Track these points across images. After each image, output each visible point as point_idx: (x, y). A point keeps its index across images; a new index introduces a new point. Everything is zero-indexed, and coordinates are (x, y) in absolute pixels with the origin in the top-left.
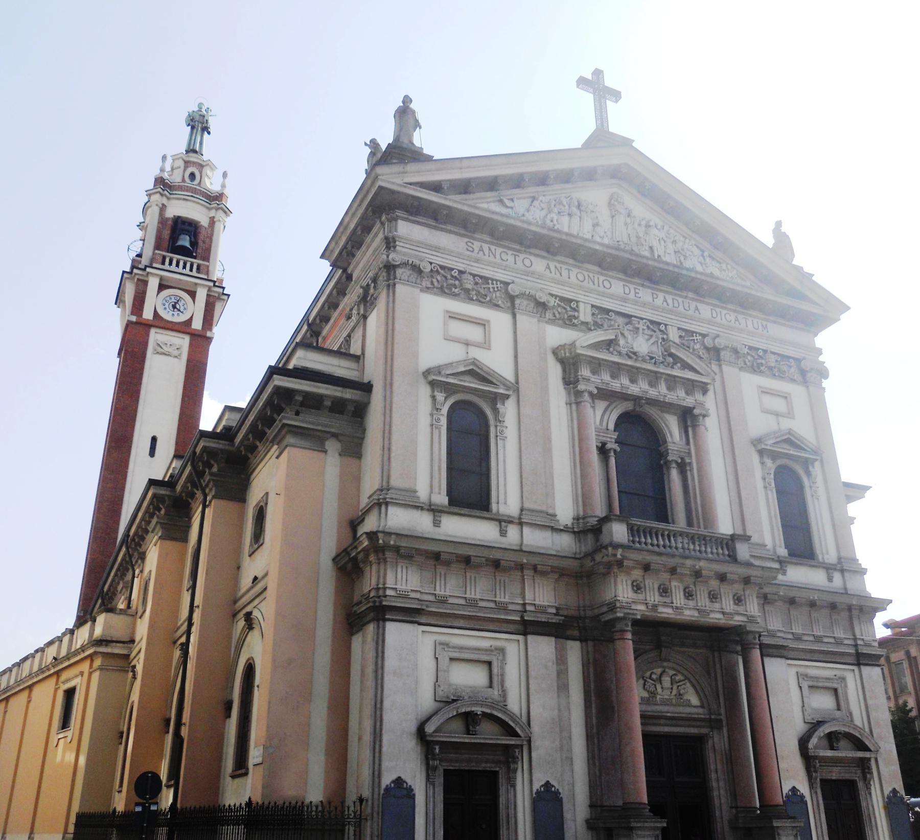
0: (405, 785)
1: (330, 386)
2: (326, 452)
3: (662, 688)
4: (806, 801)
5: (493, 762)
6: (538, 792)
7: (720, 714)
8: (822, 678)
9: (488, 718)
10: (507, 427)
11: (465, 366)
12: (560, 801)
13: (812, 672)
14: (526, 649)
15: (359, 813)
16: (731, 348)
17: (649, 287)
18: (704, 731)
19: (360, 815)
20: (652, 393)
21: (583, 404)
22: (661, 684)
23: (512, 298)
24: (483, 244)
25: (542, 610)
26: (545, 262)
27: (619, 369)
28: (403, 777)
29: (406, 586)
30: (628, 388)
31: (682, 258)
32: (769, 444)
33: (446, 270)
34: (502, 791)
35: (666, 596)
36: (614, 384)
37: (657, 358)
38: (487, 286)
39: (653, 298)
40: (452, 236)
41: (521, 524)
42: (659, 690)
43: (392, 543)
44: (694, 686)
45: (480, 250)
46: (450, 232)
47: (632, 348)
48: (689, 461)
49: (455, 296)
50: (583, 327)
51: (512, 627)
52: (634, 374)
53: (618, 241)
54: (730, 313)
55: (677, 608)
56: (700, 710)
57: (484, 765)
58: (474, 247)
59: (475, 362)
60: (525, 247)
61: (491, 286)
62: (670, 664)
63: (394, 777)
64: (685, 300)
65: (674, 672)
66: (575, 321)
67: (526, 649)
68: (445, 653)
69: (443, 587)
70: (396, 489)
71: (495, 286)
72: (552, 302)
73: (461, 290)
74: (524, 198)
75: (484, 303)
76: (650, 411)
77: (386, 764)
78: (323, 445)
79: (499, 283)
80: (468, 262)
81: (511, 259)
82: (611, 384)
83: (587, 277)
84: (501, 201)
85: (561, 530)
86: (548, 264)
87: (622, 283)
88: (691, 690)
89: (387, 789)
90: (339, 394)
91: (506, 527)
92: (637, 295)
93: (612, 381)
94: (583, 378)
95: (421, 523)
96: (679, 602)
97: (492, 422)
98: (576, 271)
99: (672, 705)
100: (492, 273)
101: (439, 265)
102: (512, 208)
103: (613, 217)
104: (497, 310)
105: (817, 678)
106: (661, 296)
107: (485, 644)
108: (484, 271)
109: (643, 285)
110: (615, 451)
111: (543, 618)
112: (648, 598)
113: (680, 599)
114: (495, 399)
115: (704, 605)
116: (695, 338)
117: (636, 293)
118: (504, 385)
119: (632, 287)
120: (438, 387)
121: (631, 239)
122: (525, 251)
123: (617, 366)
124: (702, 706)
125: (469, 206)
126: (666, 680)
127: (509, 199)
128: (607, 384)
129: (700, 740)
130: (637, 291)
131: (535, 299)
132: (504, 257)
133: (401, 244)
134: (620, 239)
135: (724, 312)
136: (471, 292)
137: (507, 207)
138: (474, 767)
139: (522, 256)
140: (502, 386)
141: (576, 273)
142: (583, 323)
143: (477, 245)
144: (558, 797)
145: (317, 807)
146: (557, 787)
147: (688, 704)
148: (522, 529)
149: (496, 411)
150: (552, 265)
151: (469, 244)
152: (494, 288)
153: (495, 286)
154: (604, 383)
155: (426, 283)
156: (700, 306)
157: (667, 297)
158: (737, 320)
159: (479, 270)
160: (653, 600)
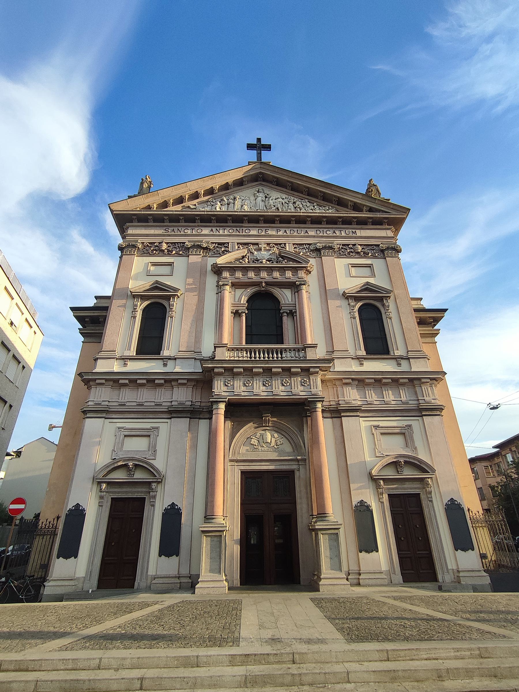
9: (409, 464)
13: (382, 424)
15: (55, 525)
18: (294, 467)
23: (382, 251)
24: (212, 228)
33: (346, 246)
37: (273, 260)
38: (175, 246)
41: (408, 359)
59: (157, 282)
61: (177, 246)
73: (355, 253)
79: (307, 245)
86: (212, 229)
92: (267, 233)
95: (355, 367)
97: (383, 311)
101: (148, 242)
107: (148, 426)
114: (381, 299)
116: (305, 247)
117: (266, 232)
120: (98, 299)
123: (258, 269)
129: (291, 473)
135: (325, 230)
136: (360, 253)
144: (460, 507)
145: (25, 520)
148: (409, 361)
149: (383, 305)
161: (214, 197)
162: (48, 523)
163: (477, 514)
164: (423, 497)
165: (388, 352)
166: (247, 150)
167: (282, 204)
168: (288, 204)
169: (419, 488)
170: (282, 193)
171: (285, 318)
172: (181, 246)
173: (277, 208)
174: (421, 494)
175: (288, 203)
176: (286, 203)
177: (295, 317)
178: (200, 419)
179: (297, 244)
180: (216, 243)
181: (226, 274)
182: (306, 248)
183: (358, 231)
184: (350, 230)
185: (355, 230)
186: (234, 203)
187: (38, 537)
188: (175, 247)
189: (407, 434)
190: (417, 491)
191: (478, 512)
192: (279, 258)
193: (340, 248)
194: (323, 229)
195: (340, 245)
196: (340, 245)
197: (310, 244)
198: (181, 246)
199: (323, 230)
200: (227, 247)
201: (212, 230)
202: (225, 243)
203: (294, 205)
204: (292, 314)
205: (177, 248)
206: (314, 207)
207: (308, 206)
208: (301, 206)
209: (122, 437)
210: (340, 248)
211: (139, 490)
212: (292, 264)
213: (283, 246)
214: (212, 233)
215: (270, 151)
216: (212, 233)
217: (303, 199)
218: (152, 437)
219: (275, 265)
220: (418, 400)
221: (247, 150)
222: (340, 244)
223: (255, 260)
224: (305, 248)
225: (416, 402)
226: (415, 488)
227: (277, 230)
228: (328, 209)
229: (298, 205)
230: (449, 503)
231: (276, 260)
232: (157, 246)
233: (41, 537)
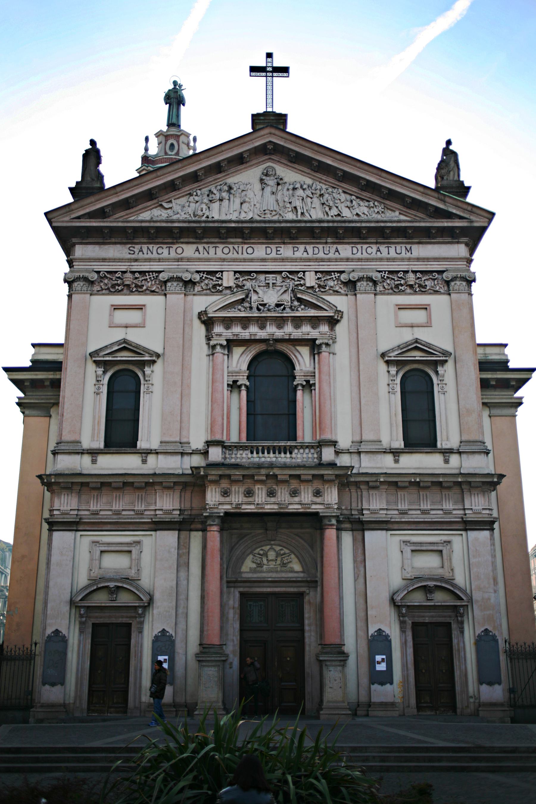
0: (61, 634)
1: (45, 373)
2: (50, 416)
3: (267, 560)
4: (498, 639)
5: (127, 617)
6: (479, 636)
7: (316, 577)
8: (426, 543)
10: (152, 385)
11: (118, 345)
12: (390, 641)
14: (156, 540)
15: (34, 651)
16: (367, 278)
17: (290, 243)
19: (35, 653)
20: (279, 333)
21: (215, 354)
22: (267, 557)
25: (168, 512)
26: (194, 246)
27: (249, 320)
28: (60, 629)
29: (67, 507)
30: (256, 335)
31: (327, 209)
32: (392, 356)
34: (134, 635)
35: (249, 497)
36: (243, 334)
37: (286, 304)
38: (145, 278)
39: (294, 251)
40: (118, 246)
42: (265, 561)
43: (53, 480)
44: (297, 557)
45: (140, 251)
46: (115, 243)
47: (263, 301)
48: (314, 382)
49: (119, 292)
50: (228, 292)
51: (146, 527)
52: (262, 322)
53: (264, 211)
54: (371, 245)
55: (258, 504)
56: (302, 575)
57: (121, 619)
58: (135, 250)
60: (176, 239)
61: (148, 277)
62: (277, 542)
63: (54, 629)
64: (325, 246)
65: (281, 548)
66: (220, 288)
67: (156, 540)
68: (98, 549)
69: (95, 504)
70: (64, 442)
71: (151, 276)
72: (197, 277)
74: (183, 196)
75: (142, 292)
76: (283, 348)
77: (49, 621)
78: (49, 412)
80: (129, 264)
81: (166, 251)
82: (241, 334)
83: (232, 249)
84: (161, 206)
85: (191, 453)
86: (197, 248)
87: (264, 246)
88: (295, 560)
89: (49, 637)
90: (51, 377)
91: (146, 457)
92: (278, 253)
93: (244, 331)
94: (216, 335)
96: (260, 500)
97: (142, 382)
98: (221, 246)
99: (277, 572)
100: (149, 267)
102: (171, 208)
103: (263, 189)
104: (155, 295)
105: (421, 543)
106: (302, 247)
108: (142, 267)
109: (284, 243)
110: (245, 385)
111: (167, 518)
112: (233, 500)
113: (262, 498)
115: (283, 499)
116: (333, 276)
117: (277, 251)
118: (149, 353)
119: (273, 247)
121: (280, 204)
122: (177, 242)
124: (303, 572)
125: (122, 222)
126: (272, 555)
127: (167, 202)
128: (237, 335)
130: (278, 249)
131: (183, 280)
132: (160, 251)
133: (77, 264)
134: (266, 209)
135: (365, 246)
137: (167, 209)
138: (114, 620)
139: (175, 246)
140: (147, 355)
141: (221, 248)
142: (227, 288)
143: (138, 247)
146: (171, 632)
147: (292, 571)
149: (437, 373)
150: (201, 247)
151: (131, 248)
152: (150, 278)
153: (151, 276)
154: (234, 335)
155: (96, 288)
156: (340, 247)
157: (308, 247)
158: (378, 250)
159: (139, 267)
160: (237, 500)
161: (199, 186)
162: (17, 649)
163: (515, 646)
164: (454, 626)
165: (435, 445)
166: (251, 76)
167: (303, 199)
168: (311, 198)
169: (450, 617)
170: (303, 175)
171: (299, 393)
172: (153, 277)
173: (295, 208)
174: (452, 623)
175: (311, 196)
176: (308, 196)
177: (313, 391)
178: (191, 530)
179: (322, 272)
180: (204, 272)
181: (218, 329)
182: (334, 279)
183: (415, 247)
184: (403, 246)
185: (410, 246)
186: (229, 200)
187: (5, 663)
188: (145, 280)
189: (444, 552)
190: (448, 620)
191: (517, 644)
192: (293, 301)
193: (385, 278)
194: (361, 245)
195: (385, 273)
196: (385, 273)
197: (342, 272)
198: (153, 277)
199: (362, 247)
200: (219, 278)
201: (197, 250)
202: (217, 272)
203: (321, 199)
204: (309, 386)
205: (149, 280)
206: (351, 201)
207: (342, 201)
208: (331, 204)
209: (98, 553)
210: (385, 278)
211: (125, 614)
212: (312, 313)
213: (301, 275)
214: (197, 255)
215: (288, 77)
216: (197, 255)
217: (335, 188)
218: (134, 552)
219: (288, 313)
220: (464, 509)
221: (251, 76)
222: (385, 271)
223: (260, 305)
224: (333, 278)
225: (462, 512)
226: (445, 617)
227: (294, 247)
228: (372, 205)
229: (327, 201)
230: (52, 634)
231: (290, 304)
232: (119, 278)
233: (17, 663)
